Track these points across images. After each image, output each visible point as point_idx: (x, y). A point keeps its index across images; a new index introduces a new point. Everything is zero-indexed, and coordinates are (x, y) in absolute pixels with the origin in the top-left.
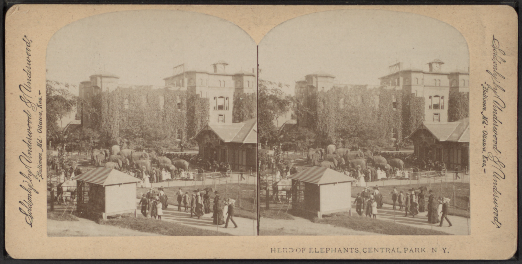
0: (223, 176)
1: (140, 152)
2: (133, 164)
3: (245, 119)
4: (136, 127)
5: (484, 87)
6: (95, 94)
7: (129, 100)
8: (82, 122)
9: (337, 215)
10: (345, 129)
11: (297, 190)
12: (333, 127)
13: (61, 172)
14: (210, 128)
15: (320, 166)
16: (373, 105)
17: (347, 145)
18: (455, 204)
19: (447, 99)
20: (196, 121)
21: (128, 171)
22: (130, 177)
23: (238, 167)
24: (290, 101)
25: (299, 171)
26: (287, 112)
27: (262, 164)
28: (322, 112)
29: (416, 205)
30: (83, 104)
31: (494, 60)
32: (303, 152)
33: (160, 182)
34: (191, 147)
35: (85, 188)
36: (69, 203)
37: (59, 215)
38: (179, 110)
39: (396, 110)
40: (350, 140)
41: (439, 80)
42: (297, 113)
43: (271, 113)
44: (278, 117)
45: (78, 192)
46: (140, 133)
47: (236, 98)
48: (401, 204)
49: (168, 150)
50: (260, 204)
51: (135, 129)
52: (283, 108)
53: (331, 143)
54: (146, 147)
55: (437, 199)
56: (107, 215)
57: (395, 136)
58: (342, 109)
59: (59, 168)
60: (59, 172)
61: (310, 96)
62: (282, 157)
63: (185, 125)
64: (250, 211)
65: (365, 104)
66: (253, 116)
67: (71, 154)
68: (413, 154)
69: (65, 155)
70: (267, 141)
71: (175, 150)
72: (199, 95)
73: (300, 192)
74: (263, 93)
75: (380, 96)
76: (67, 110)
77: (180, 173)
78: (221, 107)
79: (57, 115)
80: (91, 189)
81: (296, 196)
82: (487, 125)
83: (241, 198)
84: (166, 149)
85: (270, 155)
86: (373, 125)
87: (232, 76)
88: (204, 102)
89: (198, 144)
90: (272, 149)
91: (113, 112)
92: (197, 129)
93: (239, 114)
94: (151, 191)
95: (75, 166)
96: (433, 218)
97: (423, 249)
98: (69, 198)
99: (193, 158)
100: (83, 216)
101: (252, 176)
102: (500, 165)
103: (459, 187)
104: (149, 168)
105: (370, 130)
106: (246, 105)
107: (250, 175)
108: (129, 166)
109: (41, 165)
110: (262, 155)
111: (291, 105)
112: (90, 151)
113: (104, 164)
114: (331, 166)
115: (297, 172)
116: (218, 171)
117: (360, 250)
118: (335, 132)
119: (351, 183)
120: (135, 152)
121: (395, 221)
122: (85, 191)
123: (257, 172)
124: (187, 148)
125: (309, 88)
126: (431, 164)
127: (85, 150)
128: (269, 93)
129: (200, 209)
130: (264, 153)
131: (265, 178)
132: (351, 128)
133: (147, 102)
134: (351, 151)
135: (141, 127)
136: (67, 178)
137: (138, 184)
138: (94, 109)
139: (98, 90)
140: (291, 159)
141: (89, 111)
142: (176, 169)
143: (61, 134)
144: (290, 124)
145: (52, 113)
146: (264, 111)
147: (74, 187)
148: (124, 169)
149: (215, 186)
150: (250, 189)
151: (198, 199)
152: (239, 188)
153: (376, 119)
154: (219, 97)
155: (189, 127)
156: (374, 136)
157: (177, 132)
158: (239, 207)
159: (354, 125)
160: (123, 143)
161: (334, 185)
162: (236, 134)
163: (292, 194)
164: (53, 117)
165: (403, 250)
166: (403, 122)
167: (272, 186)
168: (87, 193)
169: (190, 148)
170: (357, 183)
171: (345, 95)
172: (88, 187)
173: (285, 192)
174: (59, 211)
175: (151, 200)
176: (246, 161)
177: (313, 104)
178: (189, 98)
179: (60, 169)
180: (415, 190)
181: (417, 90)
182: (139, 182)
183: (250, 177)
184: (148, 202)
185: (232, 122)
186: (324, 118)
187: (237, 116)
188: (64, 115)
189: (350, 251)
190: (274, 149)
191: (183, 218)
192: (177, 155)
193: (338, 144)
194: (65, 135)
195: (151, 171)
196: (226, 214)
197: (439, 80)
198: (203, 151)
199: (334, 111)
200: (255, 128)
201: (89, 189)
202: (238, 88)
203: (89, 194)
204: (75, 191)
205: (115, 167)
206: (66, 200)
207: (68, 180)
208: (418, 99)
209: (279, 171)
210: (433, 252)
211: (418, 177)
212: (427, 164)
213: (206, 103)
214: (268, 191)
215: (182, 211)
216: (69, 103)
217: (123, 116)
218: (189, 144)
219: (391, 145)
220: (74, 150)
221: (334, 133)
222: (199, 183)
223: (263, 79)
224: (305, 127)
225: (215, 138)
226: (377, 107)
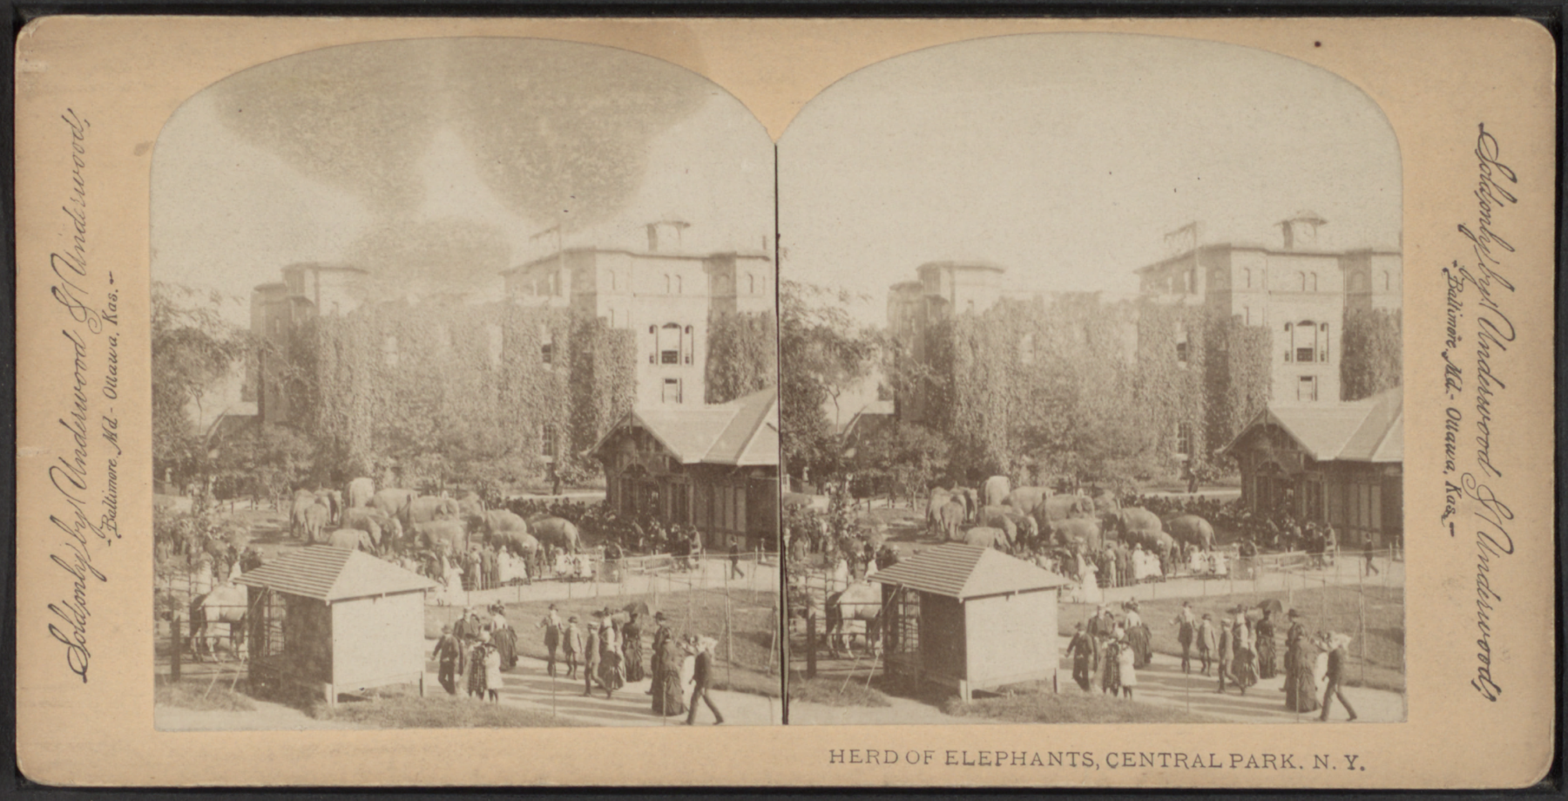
0: (680, 568)
1: (432, 497)
2: (414, 533)
3: (742, 390)
4: (419, 422)
5: (1452, 276)
6: (299, 322)
7: (398, 338)
8: (261, 408)
9: (1017, 692)
10: (1035, 427)
11: (896, 616)
12: (1000, 422)
13: (202, 562)
14: (639, 420)
15: (963, 541)
16: (1119, 355)
17: (1043, 476)
18: (1366, 652)
19: (1336, 332)
20: (598, 401)
21: (400, 554)
22: (407, 573)
23: (724, 539)
24: (874, 345)
25: (902, 559)
26: (865, 377)
27: (793, 540)
28: (968, 377)
29: (1249, 655)
30: (265, 355)
31: (1480, 195)
32: (915, 500)
33: (495, 587)
34: (582, 479)
35: (274, 610)
36: (227, 657)
37: (199, 692)
38: (547, 367)
39: (1188, 366)
40: (1053, 462)
41: (1314, 274)
42: (896, 384)
43: (816, 381)
44: (839, 394)
45: (252, 624)
46: (432, 440)
47: (716, 327)
48: (1206, 654)
49: (518, 488)
50: (790, 661)
51: (419, 427)
52: (853, 367)
53: (994, 470)
54: (452, 481)
55: (1311, 636)
56: (338, 691)
57: (1186, 448)
58: (1029, 367)
59: (193, 550)
60: (193, 561)
61: (932, 327)
62: (851, 518)
63: (566, 412)
64: (759, 672)
65: (1094, 350)
66: (766, 383)
67: (229, 507)
68: (1239, 500)
69: (211, 511)
70: (806, 469)
71: (536, 490)
72: (605, 319)
73: (907, 621)
74: (793, 321)
75: (1138, 324)
76: (215, 371)
77: (551, 558)
78: (670, 357)
79: (188, 387)
80: (290, 611)
81: (895, 635)
82: (1460, 390)
83: (734, 634)
84: (508, 485)
85: (817, 511)
86: (1119, 415)
87: (704, 259)
88: (620, 342)
89: (606, 472)
90: (823, 494)
91: (352, 377)
92: (601, 425)
93: (723, 375)
94: (469, 615)
95: (242, 545)
96: (1300, 696)
97: (1286, 758)
98: (225, 642)
99: (589, 514)
100: (267, 696)
101: (764, 564)
102: (1499, 514)
103: (1378, 599)
104: (461, 547)
105: (1109, 429)
106: (745, 349)
107: (760, 563)
108: (401, 540)
109: (115, 497)
110: (793, 512)
111: (875, 356)
112: (286, 497)
113: (328, 536)
114: (996, 542)
115: (896, 561)
116: (665, 551)
117: (1099, 758)
118: (1009, 436)
119: (1055, 592)
120: (419, 496)
121: (1188, 707)
122: (273, 619)
123: (779, 554)
124: (572, 482)
125: (929, 302)
126: (1291, 530)
127: (272, 494)
128: (810, 321)
129: (613, 669)
130: (799, 505)
131: (802, 579)
132: (1054, 424)
133: (453, 343)
134: (1054, 494)
135: (435, 420)
136: (219, 580)
137: (429, 594)
138: (297, 368)
139: (309, 311)
140: (880, 523)
141: (281, 374)
142: (541, 547)
143: (199, 447)
144: (874, 416)
145: (172, 382)
146: (798, 377)
147: (239, 606)
148: (387, 549)
149: (657, 597)
150: (760, 604)
151: (606, 639)
152: (729, 602)
153: (1128, 397)
154: (665, 323)
155: (576, 417)
156: (1123, 447)
157: (541, 433)
158: (727, 659)
159: (1062, 415)
160: (384, 469)
161: (1007, 598)
162: (716, 438)
163: (885, 629)
164: (176, 393)
165: (1228, 762)
166: (1208, 405)
167: (823, 607)
168: (277, 624)
169: (582, 484)
170: (1076, 592)
171: (1035, 322)
172: (282, 606)
173: (863, 623)
174: (197, 681)
175: (468, 645)
176: (749, 519)
177: (941, 353)
178: (575, 330)
179: (197, 551)
180: (1246, 611)
181: (1250, 307)
182: (431, 589)
183: (760, 568)
184: (457, 649)
185: (702, 400)
186: (975, 394)
187: (720, 382)
188: (207, 388)
189: (1067, 760)
190: (830, 493)
191: (564, 696)
192: (543, 504)
193: (1018, 475)
194: (211, 448)
195: (466, 555)
196: (690, 683)
197: (1314, 274)
198: (620, 499)
199: (1004, 372)
200: (773, 417)
201: (284, 613)
202: (719, 298)
203: (284, 629)
204: (243, 618)
205: (360, 542)
206: (218, 648)
207: (221, 584)
208: (1251, 332)
209: (845, 559)
210: (1316, 767)
211: (1254, 571)
212: (1282, 529)
213: (627, 345)
214: (811, 623)
215: (561, 675)
216: (221, 351)
217: (383, 387)
218: (578, 469)
219: (1172, 474)
220: (239, 495)
221: (1005, 441)
222: (608, 590)
223: (794, 279)
224: (921, 422)
225: (653, 451)
226: (1131, 360)
